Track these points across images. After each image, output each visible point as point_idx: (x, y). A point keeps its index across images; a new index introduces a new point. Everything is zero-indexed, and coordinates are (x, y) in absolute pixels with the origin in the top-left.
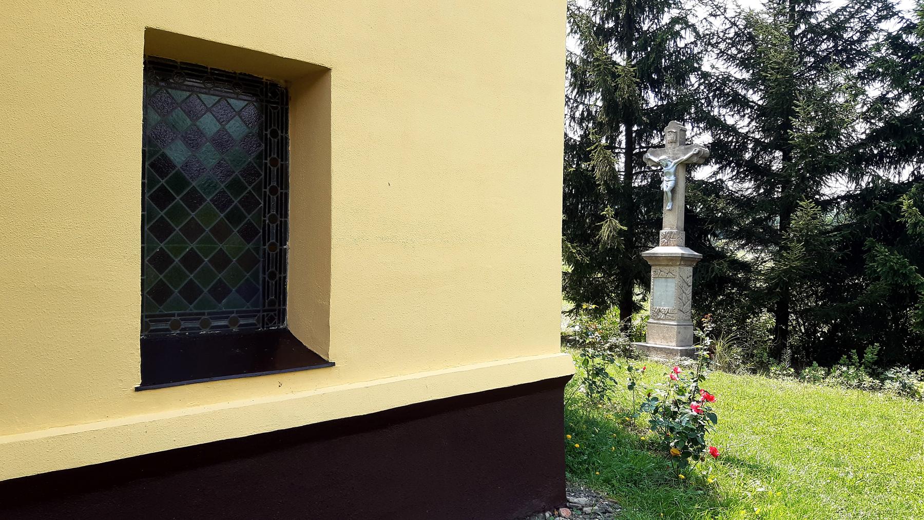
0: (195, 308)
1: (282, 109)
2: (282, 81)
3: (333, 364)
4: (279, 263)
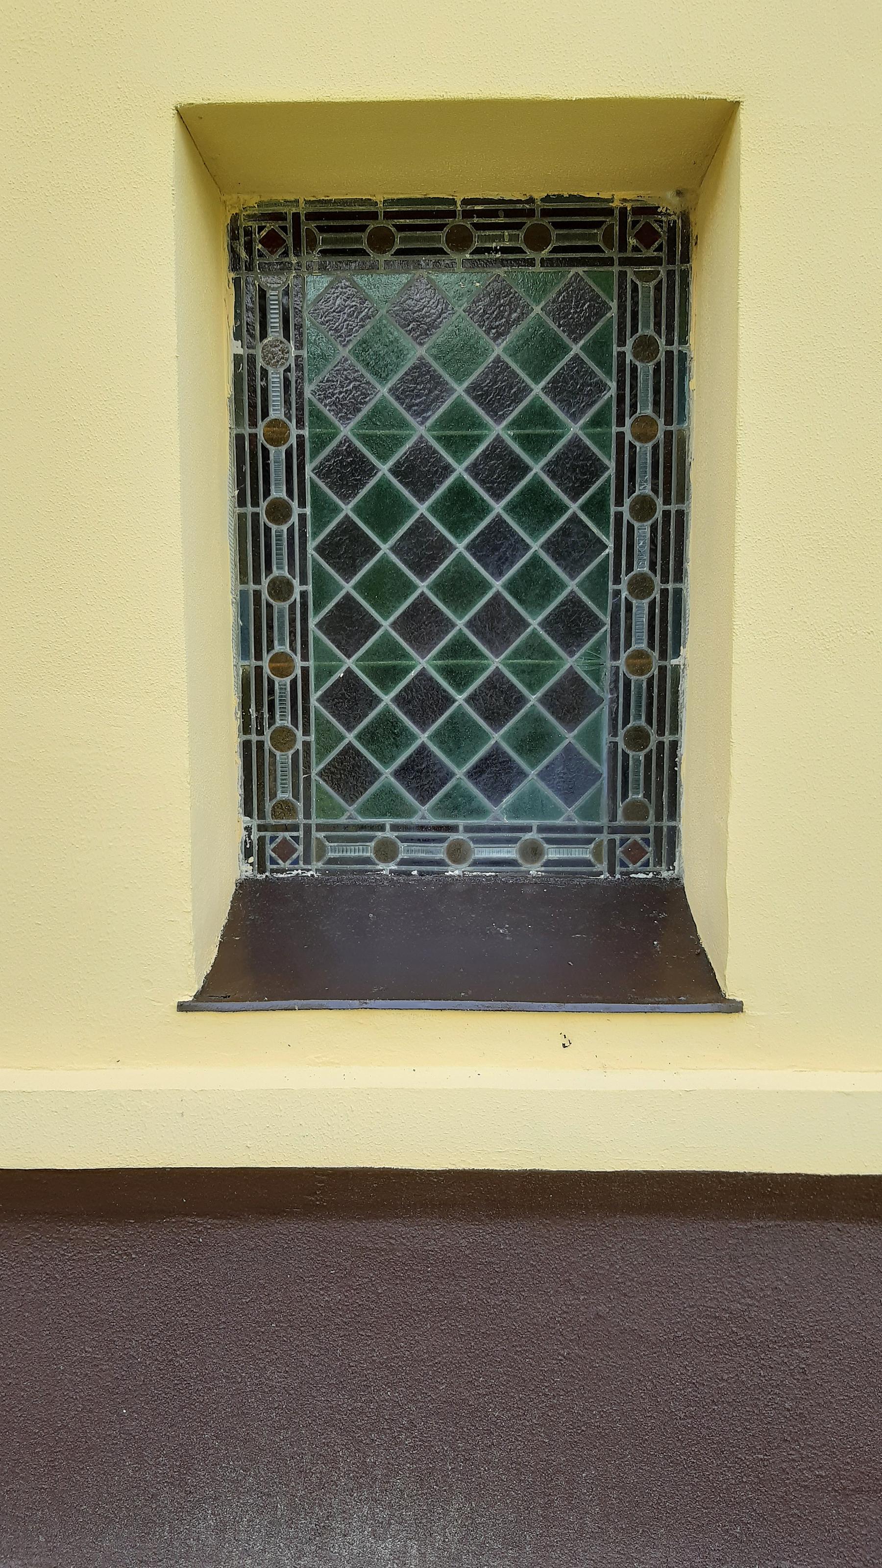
0: (364, 811)
1: (670, 274)
2: (670, 195)
3: (736, 1007)
4: (658, 703)
